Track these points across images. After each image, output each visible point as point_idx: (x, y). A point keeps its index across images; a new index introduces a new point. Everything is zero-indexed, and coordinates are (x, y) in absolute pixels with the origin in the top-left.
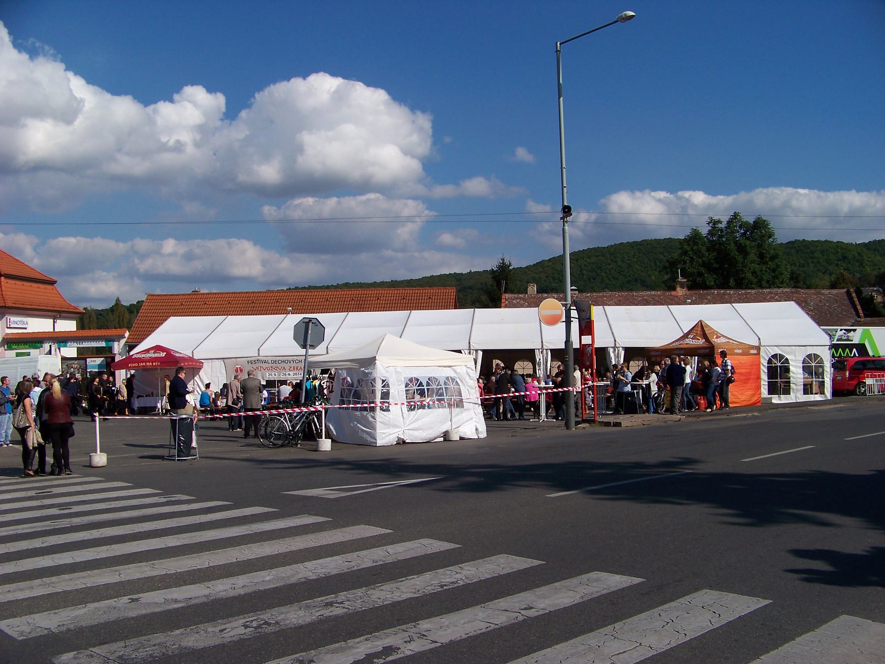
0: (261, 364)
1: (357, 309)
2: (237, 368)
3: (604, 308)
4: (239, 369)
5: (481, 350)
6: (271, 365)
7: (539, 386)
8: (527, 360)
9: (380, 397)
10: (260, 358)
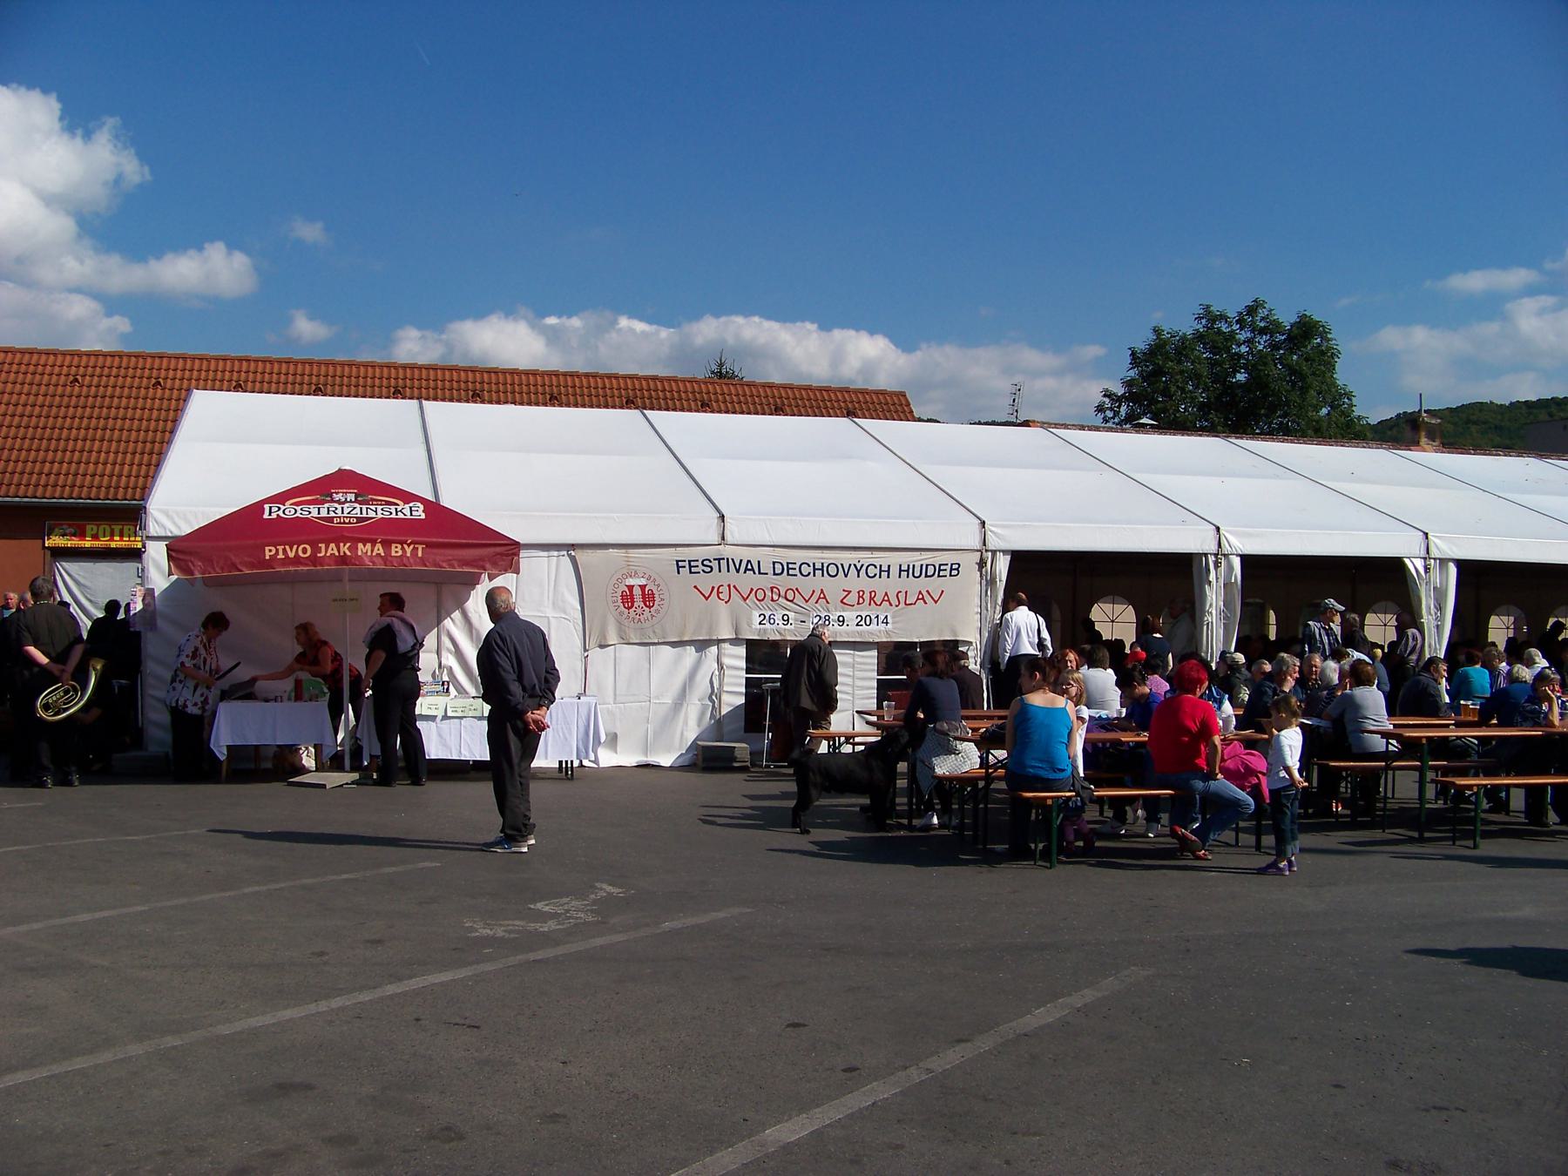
0: (732, 577)
1: (384, 390)
2: (631, 588)
3: (421, 408)
4: (637, 592)
5: (1005, 552)
6: (768, 581)
7: (294, 676)
8: (1121, 599)
9: (1007, 736)
10: (727, 552)
